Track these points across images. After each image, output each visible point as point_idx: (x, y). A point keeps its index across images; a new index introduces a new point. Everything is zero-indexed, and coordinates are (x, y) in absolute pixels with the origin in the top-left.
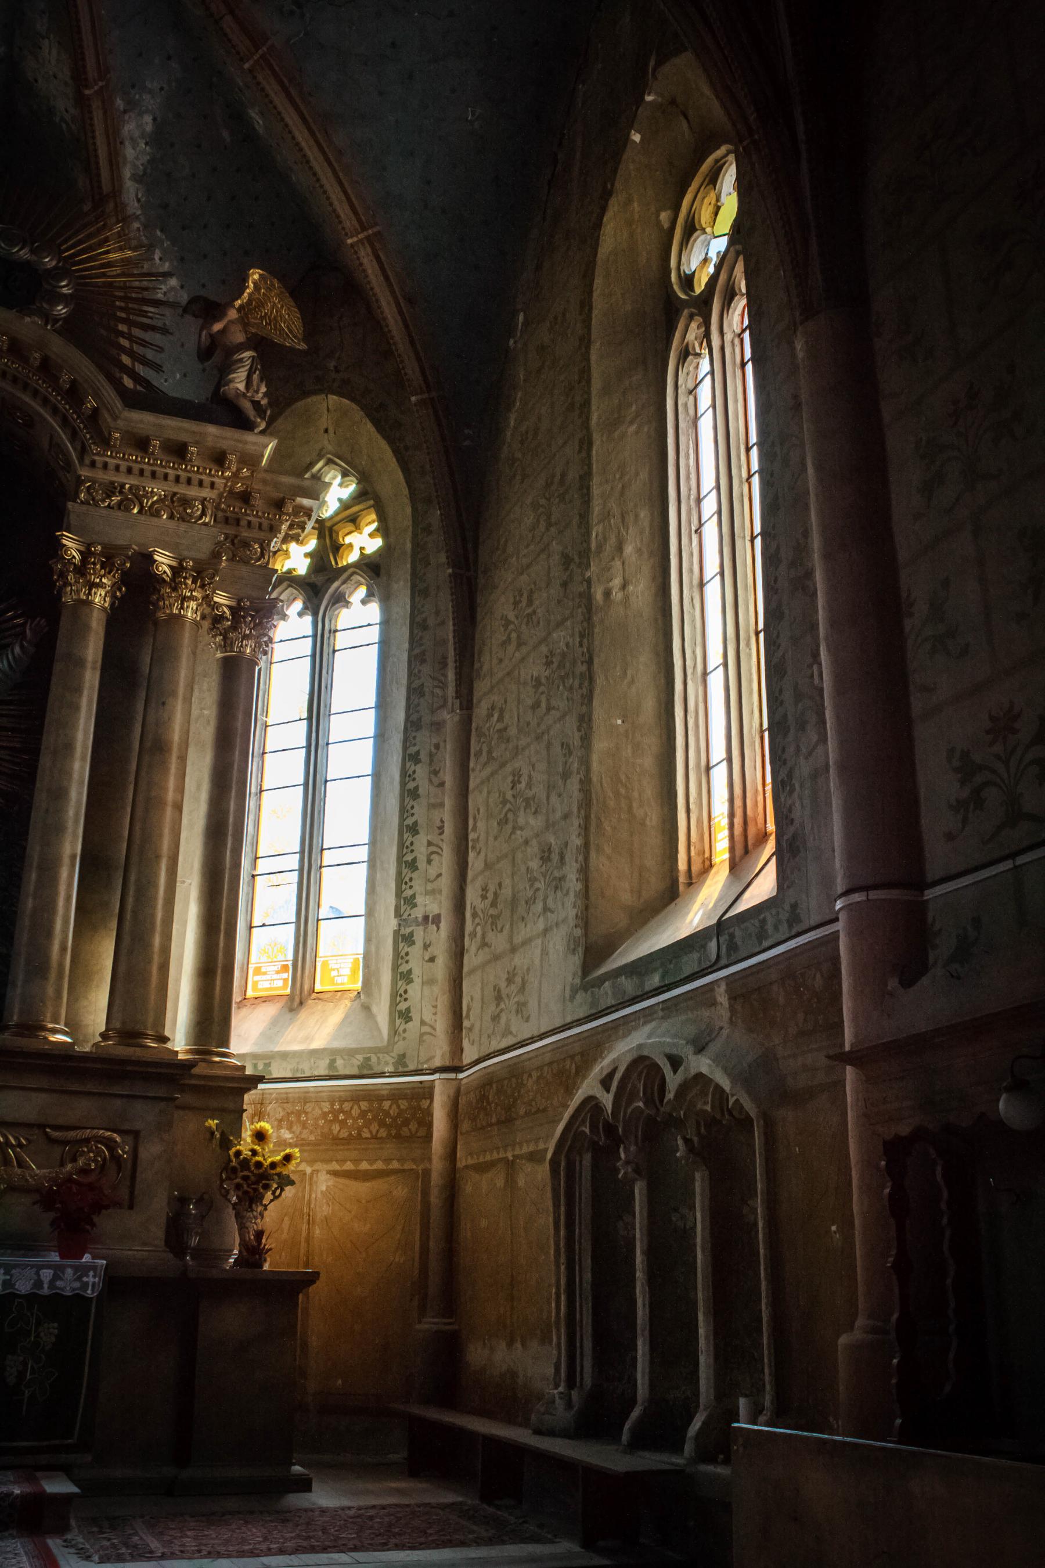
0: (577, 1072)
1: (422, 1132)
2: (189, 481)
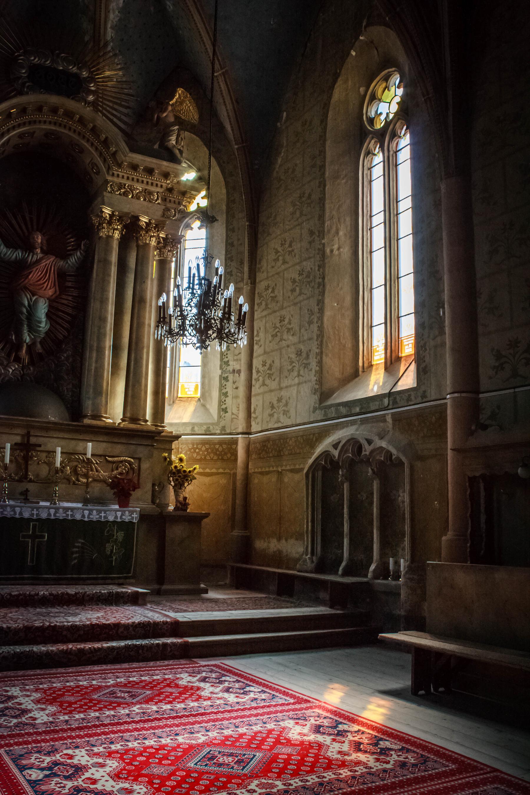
0: (317, 440)
1: (233, 458)
2: (152, 184)
